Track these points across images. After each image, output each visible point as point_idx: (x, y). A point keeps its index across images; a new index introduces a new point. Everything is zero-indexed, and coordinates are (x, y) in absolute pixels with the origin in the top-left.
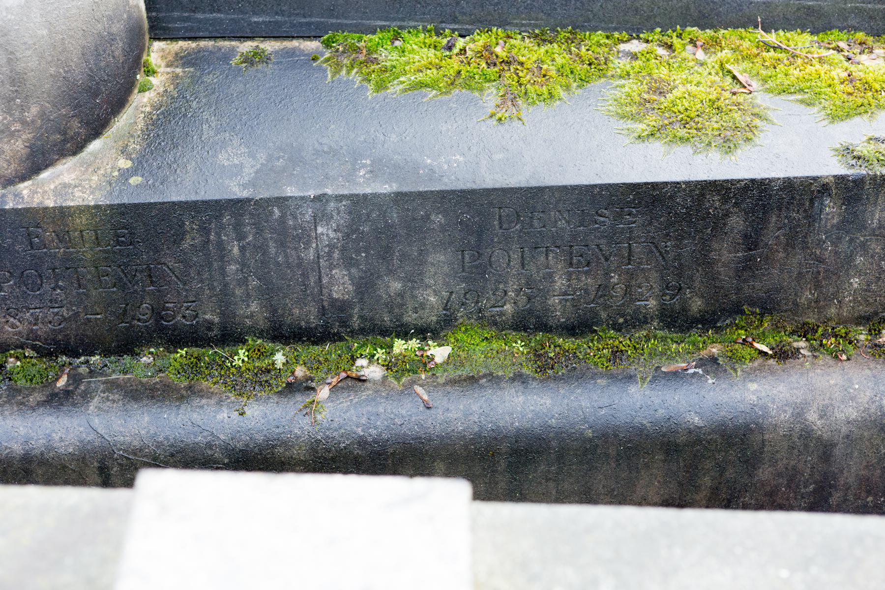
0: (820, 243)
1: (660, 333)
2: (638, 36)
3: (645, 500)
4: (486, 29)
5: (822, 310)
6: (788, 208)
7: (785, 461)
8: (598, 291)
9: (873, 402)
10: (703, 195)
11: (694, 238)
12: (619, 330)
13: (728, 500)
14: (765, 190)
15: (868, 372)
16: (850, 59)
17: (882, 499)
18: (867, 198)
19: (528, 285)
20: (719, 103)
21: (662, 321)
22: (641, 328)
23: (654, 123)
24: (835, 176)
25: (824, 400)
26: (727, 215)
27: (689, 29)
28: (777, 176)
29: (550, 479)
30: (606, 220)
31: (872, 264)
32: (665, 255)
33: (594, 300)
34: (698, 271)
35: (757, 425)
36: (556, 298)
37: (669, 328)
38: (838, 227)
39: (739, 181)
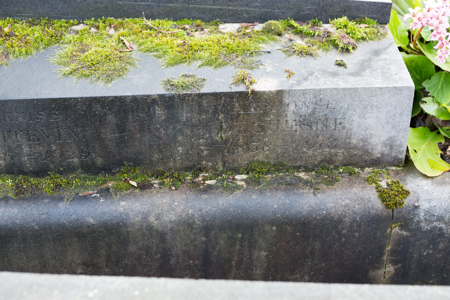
0: (158, 129)
1: (83, 176)
2: (83, 22)
3: (73, 262)
4: (4, 19)
5: (166, 164)
6: (137, 111)
7: (142, 242)
8: (47, 154)
9: (184, 212)
10: (91, 104)
11: (91, 127)
12: (62, 174)
13: (116, 262)
14: (123, 102)
15: (184, 196)
16: (188, 34)
17: (198, 262)
18: (177, 106)
19: (10, 150)
20: (110, 57)
21: (82, 169)
22: (73, 173)
23: (73, 67)
24: (158, 95)
25: (158, 210)
26: (105, 115)
27: (109, 18)
28: (128, 95)
29: (21, 251)
30: (43, 117)
31: (187, 140)
32: (78, 135)
33: (45, 159)
34: (96, 144)
35: (123, 223)
36: (26, 157)
37: (87, 172)
38: (166, 121)
39: (109, 97)
